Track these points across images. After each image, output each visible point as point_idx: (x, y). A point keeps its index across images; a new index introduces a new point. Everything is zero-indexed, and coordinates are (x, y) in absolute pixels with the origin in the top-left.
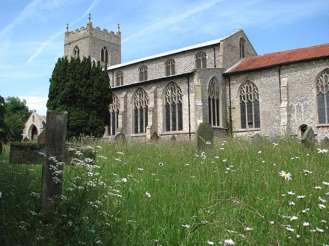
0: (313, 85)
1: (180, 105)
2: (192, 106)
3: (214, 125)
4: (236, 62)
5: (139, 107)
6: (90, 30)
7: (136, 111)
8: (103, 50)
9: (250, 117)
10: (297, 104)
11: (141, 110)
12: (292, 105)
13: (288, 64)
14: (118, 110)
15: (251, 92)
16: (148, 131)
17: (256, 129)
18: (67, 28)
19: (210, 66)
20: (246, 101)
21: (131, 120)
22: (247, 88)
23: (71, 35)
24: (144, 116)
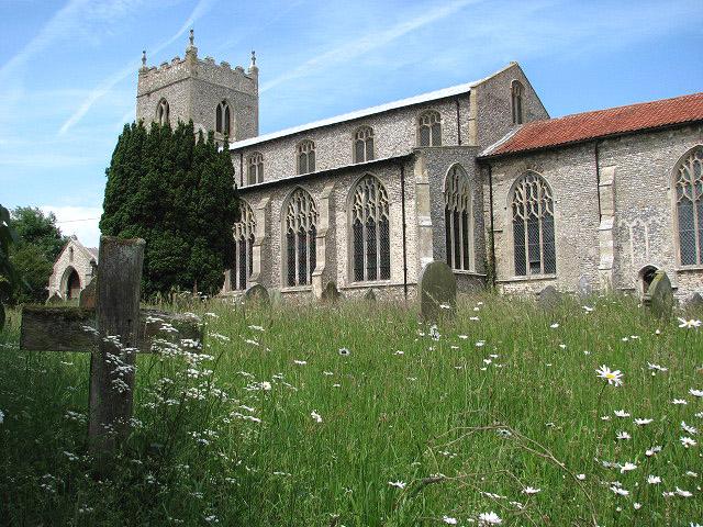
0: (670, 182)
1: (385, 225)
2: (411, 228)
3: (458, 267)
4: (504, 134)
5: (296, 230)
6: (193, 64)
7: (291, 237)
8: (219, 106)
9: (534, 250)
10: (634, 224)
11: (302, 236)
12: (623, 224)
13: (615, 138)
14: (252, 236)
15: (536, 196)
16: (317, 281)
17: (548, 276)
18: (144, 59)
19: (448, 141)
20: (525, 217)
21: (280, 257)
22: (528, 188)
23: (152, 75)
24: (308, 249)
